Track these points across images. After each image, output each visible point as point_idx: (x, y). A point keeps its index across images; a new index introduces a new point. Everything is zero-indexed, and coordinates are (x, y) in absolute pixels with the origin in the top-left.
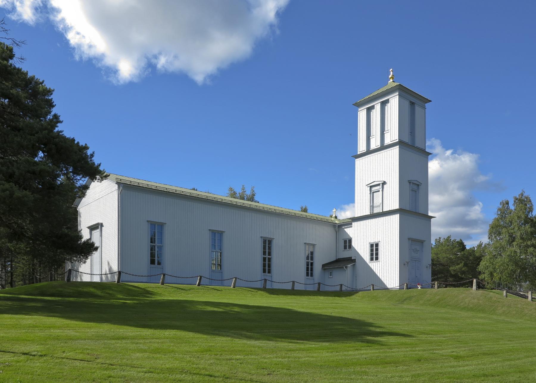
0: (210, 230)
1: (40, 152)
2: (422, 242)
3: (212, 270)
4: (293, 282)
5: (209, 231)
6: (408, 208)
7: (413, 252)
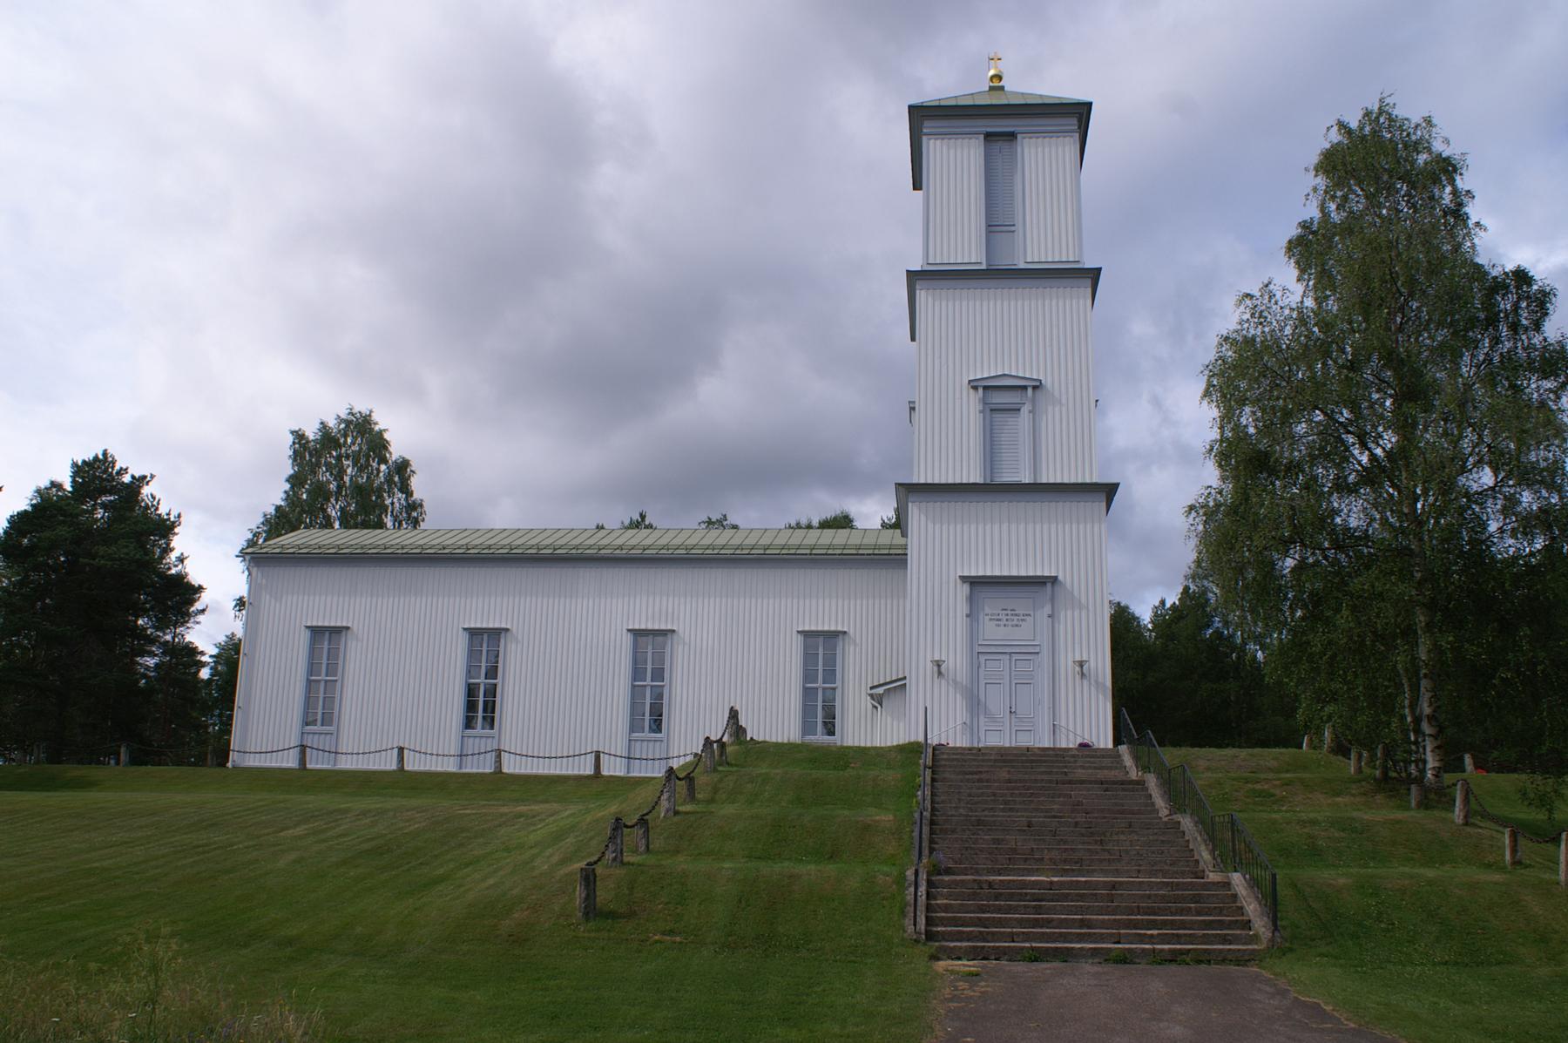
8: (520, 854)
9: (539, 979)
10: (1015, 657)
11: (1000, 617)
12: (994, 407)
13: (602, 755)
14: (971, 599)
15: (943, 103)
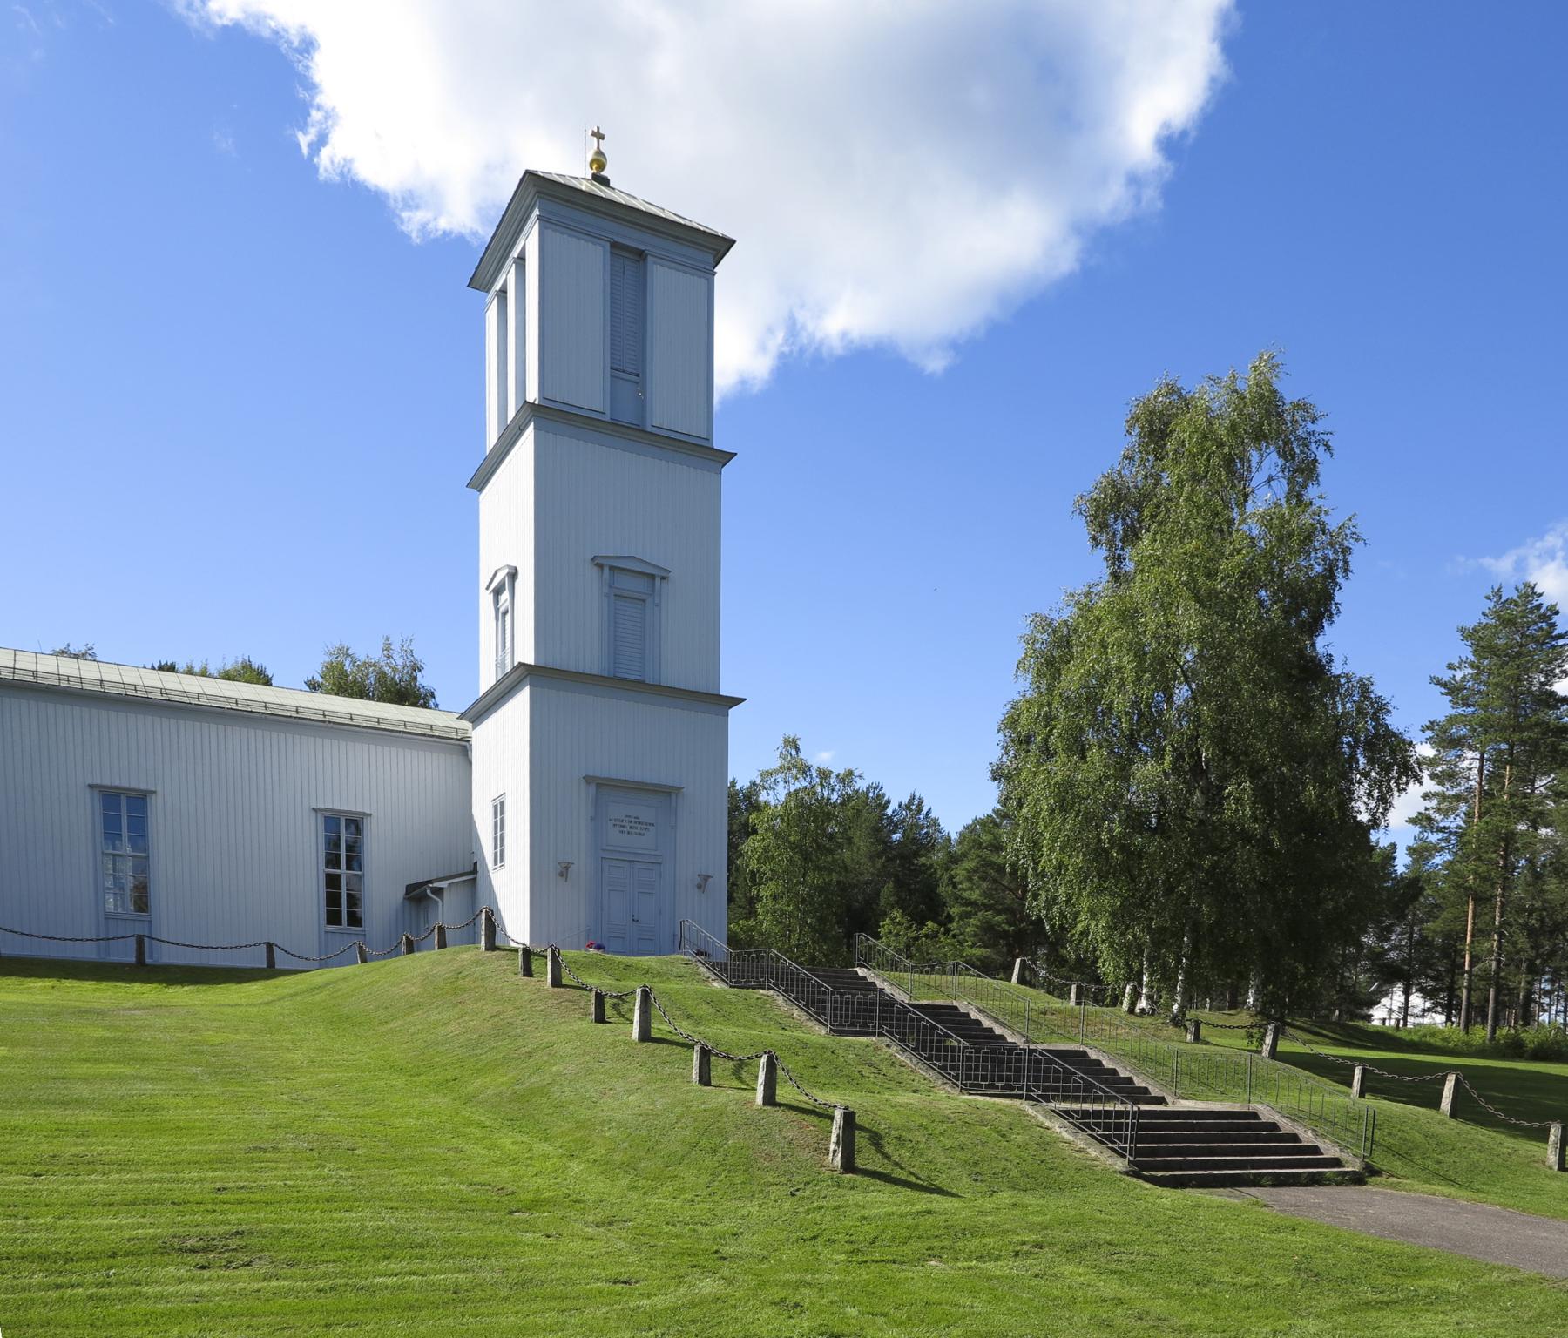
0: (90, 786)
1: (1407, 867)
2: (669, 794)
3: (106, 913)
4: (270, 946)
5: (88, 791)
6: (590, 659)
7: (617, 828)
8: (370, 1064)
9: (310, 1187)
10: (638, 865)
11: (624, 823)
12: (619, 592)
13: (146, 940)
14: (596, 803)
15: (546, 176)
